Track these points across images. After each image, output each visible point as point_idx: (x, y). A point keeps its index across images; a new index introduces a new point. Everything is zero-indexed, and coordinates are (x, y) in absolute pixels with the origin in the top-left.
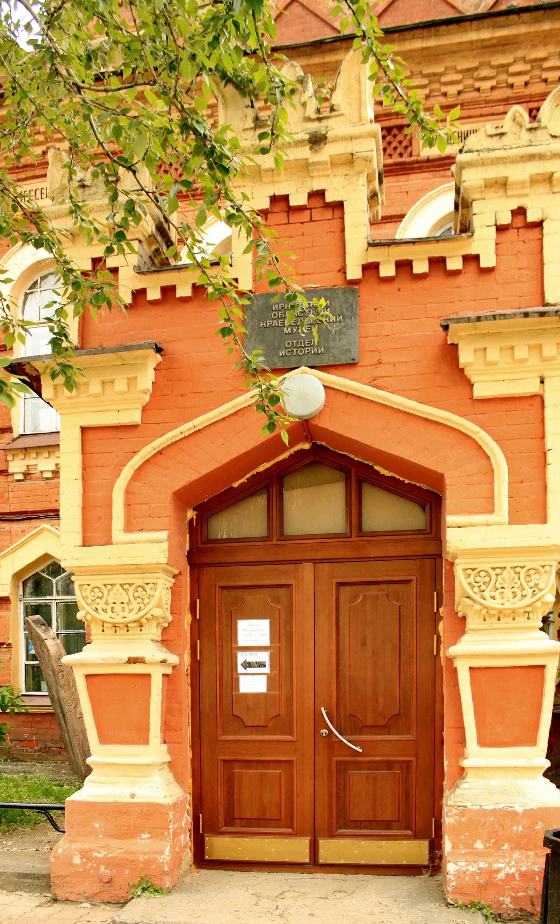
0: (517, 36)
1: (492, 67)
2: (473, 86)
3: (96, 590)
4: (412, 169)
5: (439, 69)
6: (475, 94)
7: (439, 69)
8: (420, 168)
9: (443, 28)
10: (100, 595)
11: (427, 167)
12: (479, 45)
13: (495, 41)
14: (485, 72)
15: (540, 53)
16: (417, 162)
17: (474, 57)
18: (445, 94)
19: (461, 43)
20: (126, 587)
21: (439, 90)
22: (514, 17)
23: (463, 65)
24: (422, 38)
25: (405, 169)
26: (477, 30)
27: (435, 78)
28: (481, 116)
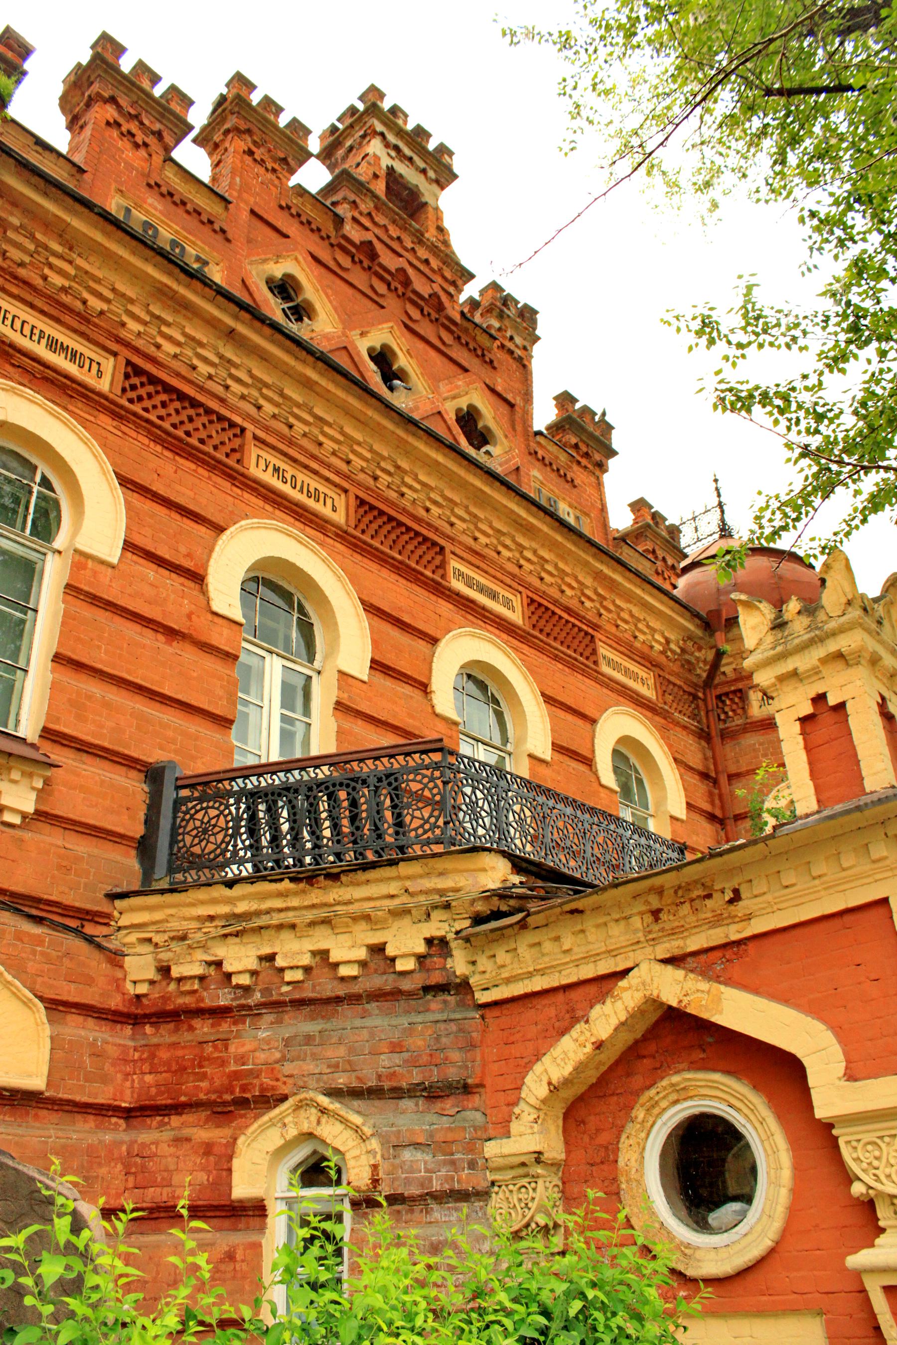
0: (540, 530)
1: (185, 334)
2: (287, 419)
3: (869, 1147)
4: (443, 593)
5: (481, 515)
6: (495, 555)
7: (358, 436)
8: (449, 596)
9: (498, 484)
10: (877, 1153)
11: (454, 600)
12: (514, 517)
13: (524, 523)
14: (508, 542)
15: (358, 436)
16: (243, 475)
17: (505, 523)
18: (476, 539)
19: (506, 507)
20: (854, 1144)
21: (225, 380)
22: (542, 514)
23: (498, 525)
24: (475, 475)
25: (437, 590)
26: (445, 455)
27: (193, 344)
28: (494, 577)
